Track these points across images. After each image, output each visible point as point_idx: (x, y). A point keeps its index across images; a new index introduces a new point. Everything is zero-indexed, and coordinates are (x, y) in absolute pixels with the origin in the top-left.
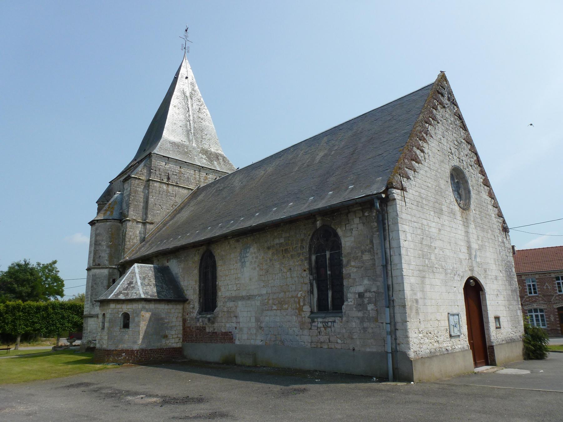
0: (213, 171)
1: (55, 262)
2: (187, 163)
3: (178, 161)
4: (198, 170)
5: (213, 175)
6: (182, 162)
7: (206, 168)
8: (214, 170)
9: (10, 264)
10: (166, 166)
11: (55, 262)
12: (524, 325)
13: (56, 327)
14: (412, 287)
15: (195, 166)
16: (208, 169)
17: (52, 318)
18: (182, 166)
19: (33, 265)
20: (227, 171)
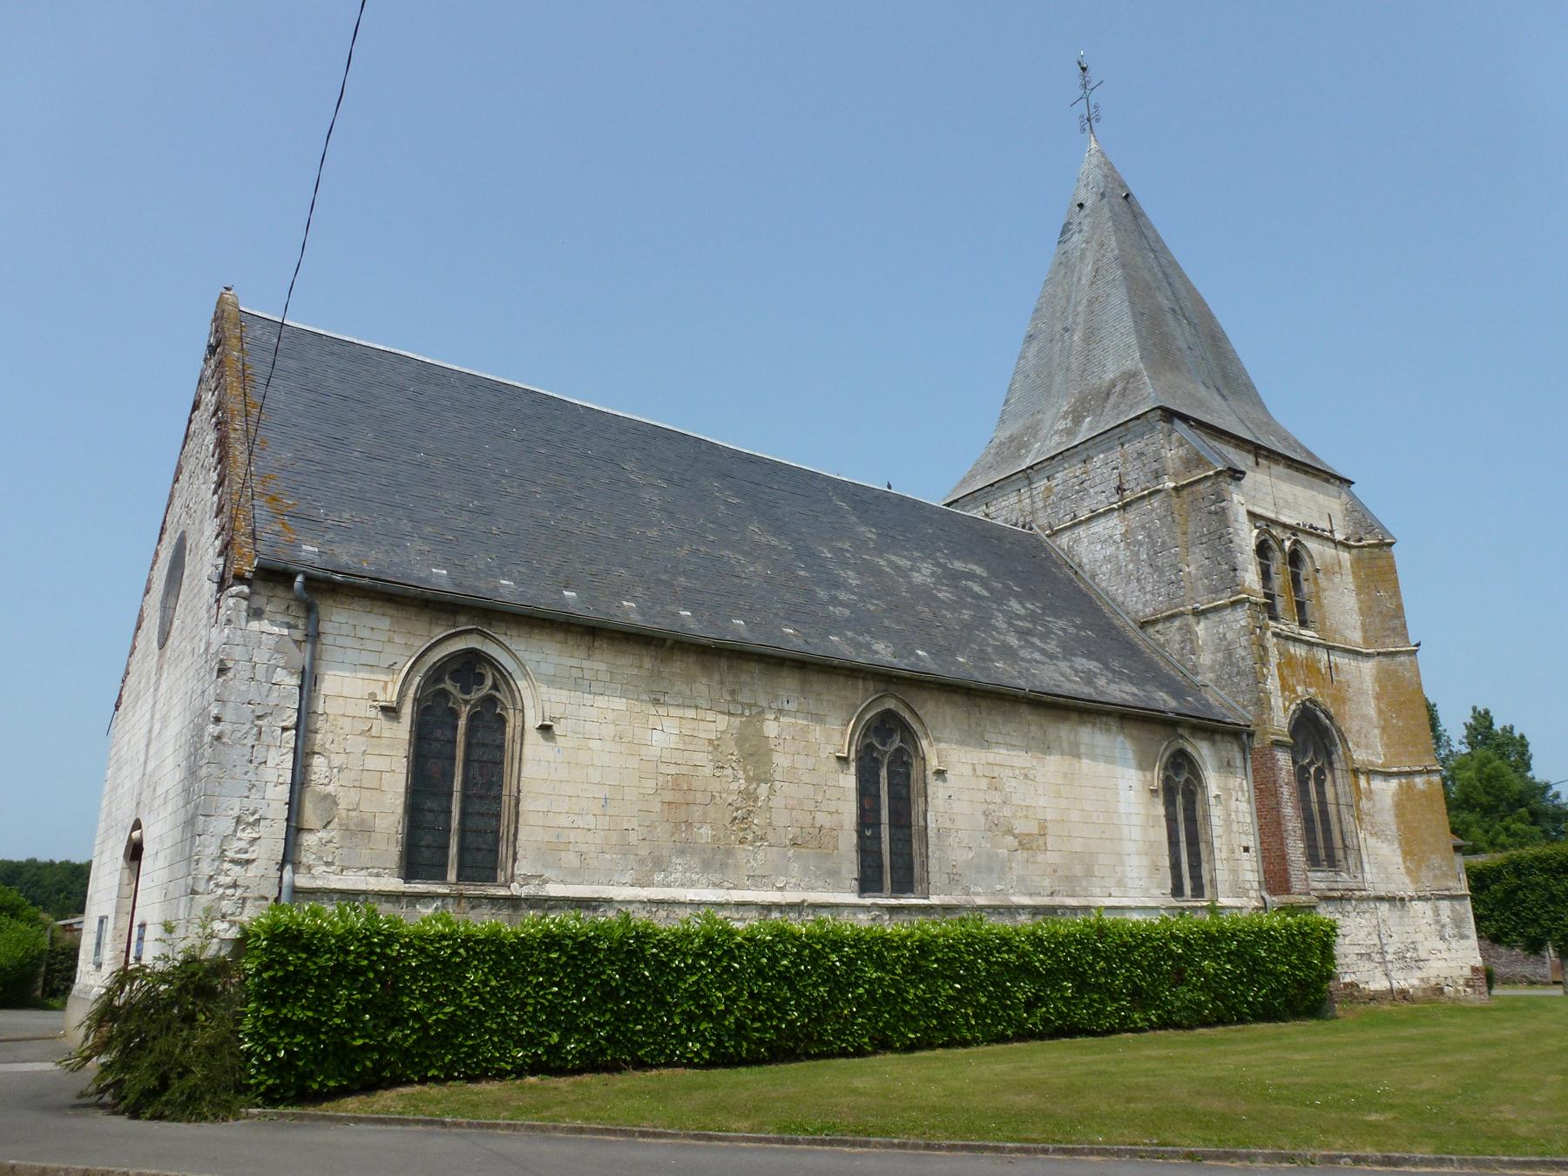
0: (1060, 457)
1: (1474, 709)
2: (996, 485)
3: (975, 495)
4: (1026, 482)
5: (1065, 469)
6: (985, 491)
7: (1039, 466)
8: (1061, 453)
9: (30, 857)
10: (248, 875)
11: (1474, 709)
12: (956, 744)
13: (1541, 926)
14: (61, 891)
15: (1014, 478)
16: (1045, 464)
17: (1524, 901)
18: (988, 500)
19: (1445, 730)
20: (1118, 419)
